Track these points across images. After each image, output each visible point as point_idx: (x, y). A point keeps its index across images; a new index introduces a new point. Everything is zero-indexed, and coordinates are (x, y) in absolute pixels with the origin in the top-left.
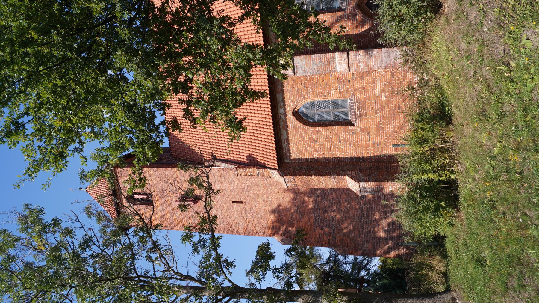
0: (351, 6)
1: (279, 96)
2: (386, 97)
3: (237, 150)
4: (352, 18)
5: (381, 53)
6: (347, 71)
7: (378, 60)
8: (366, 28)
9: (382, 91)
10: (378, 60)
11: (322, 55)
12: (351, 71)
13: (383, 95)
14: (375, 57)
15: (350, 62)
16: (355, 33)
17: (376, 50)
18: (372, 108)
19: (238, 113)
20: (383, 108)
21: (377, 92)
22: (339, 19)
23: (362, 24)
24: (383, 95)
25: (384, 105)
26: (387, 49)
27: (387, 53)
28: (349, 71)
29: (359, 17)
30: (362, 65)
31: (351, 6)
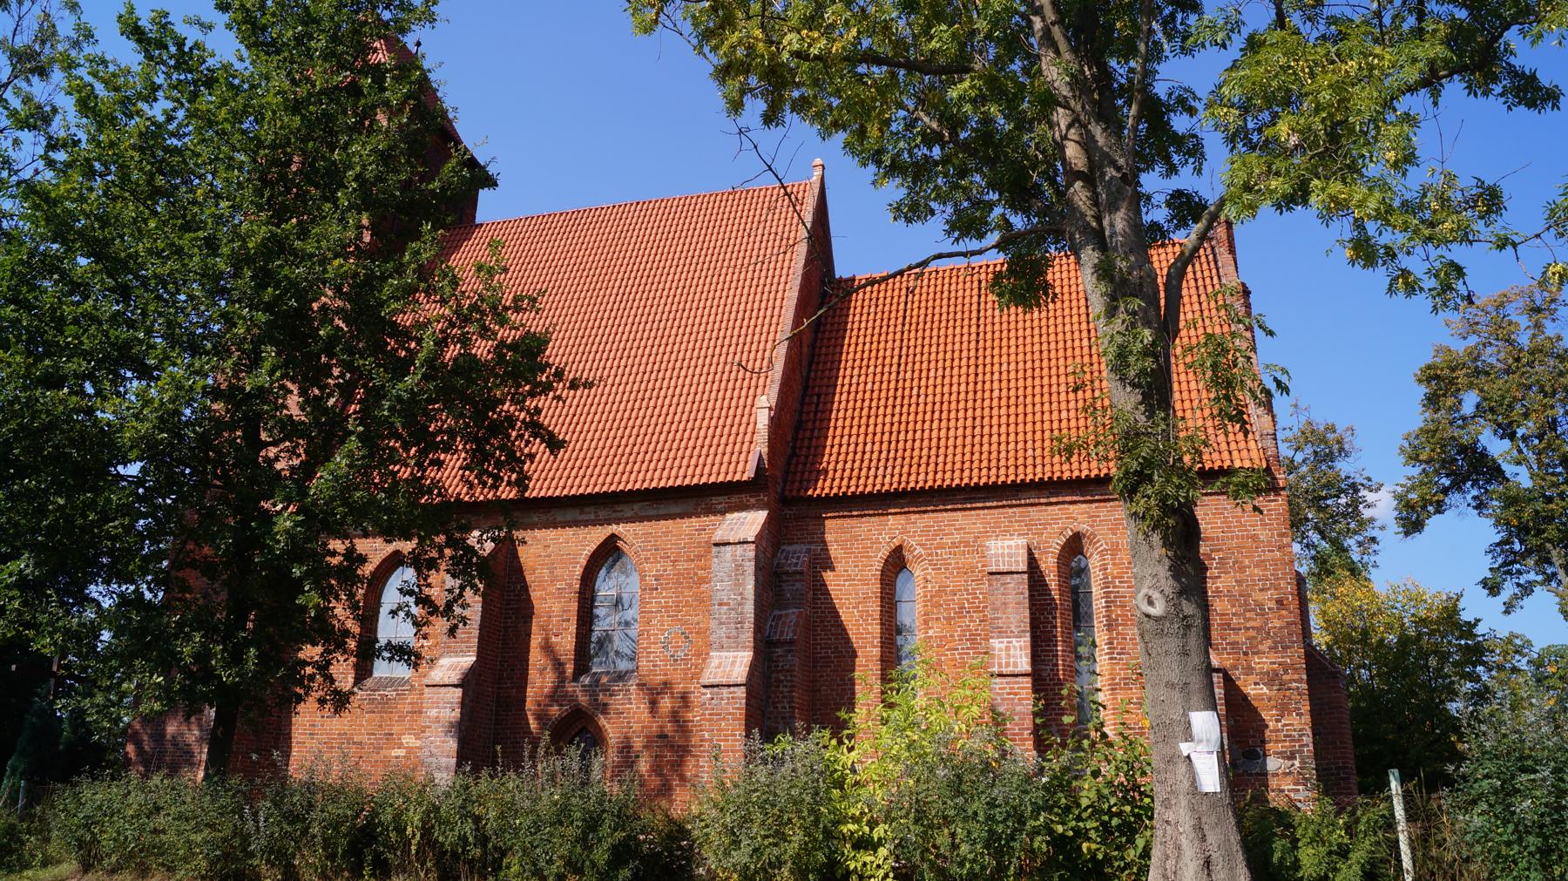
0: (580, 694)
1: (571, 515)
2: (397, 757)
3: (726, 458)
4: (557, 695)
5: (448, 756)
6: (706, 682)
7: (437, 747)
8: (533, 724)
9: (410, 750)
10: (437, 747)
11: (877, 641)
12: (427, 690)
13: (401, 752)
14: (443, 742)
15: (443, 690)
16: (528, 699)
17: (455, 746)
18: (381, 726)
19: (586, 391)
20: (378, 749)
21: (409, 740)
22: (558, 665)
23: (541, 717)
24: (401, 752)
25: (383, 752)
26: (453, 769)
27: (447, 768)
28: (705, 687)
29: (555, 710)
30: (433, 713)
31: (580, 694)
